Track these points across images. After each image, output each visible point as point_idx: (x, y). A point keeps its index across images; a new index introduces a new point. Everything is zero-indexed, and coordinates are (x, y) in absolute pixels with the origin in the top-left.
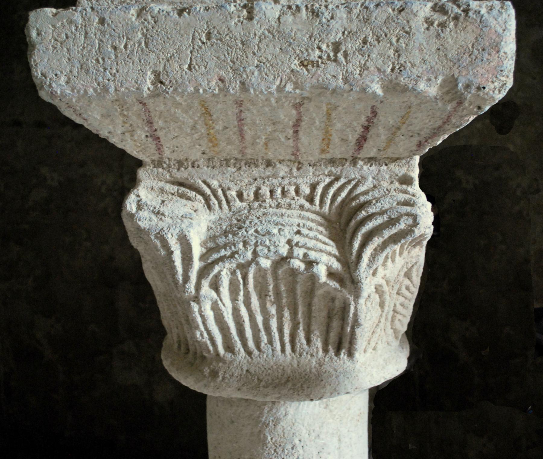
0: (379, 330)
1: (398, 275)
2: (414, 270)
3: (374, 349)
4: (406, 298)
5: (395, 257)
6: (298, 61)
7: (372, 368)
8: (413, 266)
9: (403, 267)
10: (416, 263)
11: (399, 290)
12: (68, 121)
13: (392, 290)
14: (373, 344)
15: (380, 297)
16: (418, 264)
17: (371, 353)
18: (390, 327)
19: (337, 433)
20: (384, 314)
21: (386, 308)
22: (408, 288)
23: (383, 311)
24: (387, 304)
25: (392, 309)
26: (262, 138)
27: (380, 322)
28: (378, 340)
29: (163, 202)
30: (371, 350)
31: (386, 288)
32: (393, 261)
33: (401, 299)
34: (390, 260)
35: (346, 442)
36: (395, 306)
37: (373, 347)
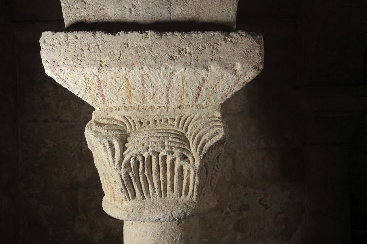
0: (205, 186)
1: (214, 159)
2: (220, 156)
3: (204, 195)
4: (216, 171)
5: (213, 150)
6: (163, 67)
7: (203, 203)
8: (219, 155)
9: (215, 156)
10: (221, 154)
11: (214, 166)
12: (120, 151)
13: (211, 166)
14: (203, 192)
15: (206, 169)
16: (221, 155)
17: (202, 197)
18: (210, 185)
19: (187, 237)
20: (208, 178)
21: (209, 175)
22: (217, 167)
23: (207, 176)
24: (209, 173)
25: (210, 176)
26: (146, 143)
27: (206, 181)
28: (205, 191)
29: (192, 225)
30: (202, 196)
31: (208, 165)
32: (212, 152)
33: (214, 171)
34: (211, 151)
35: (191, 242)
36: (212, 174)
37: (203, 194)
